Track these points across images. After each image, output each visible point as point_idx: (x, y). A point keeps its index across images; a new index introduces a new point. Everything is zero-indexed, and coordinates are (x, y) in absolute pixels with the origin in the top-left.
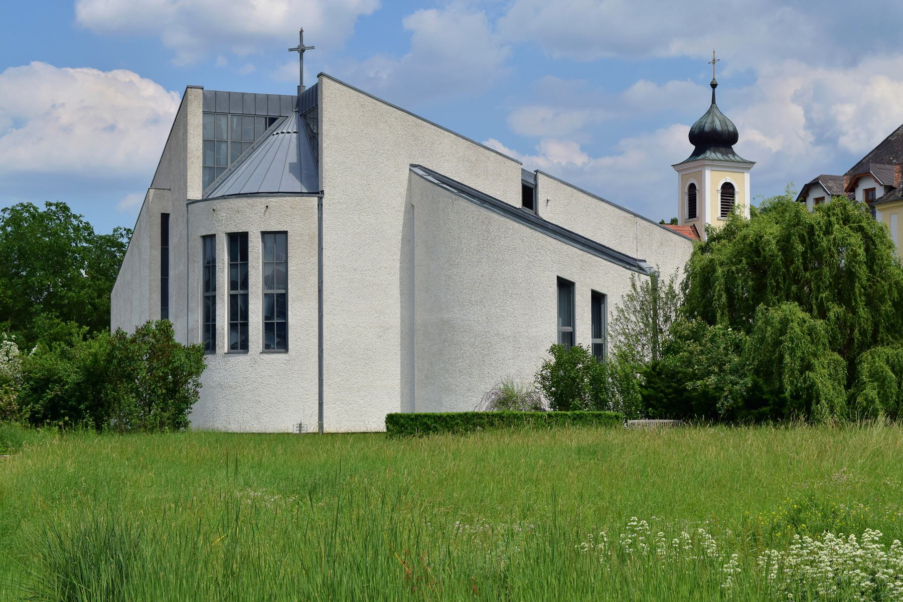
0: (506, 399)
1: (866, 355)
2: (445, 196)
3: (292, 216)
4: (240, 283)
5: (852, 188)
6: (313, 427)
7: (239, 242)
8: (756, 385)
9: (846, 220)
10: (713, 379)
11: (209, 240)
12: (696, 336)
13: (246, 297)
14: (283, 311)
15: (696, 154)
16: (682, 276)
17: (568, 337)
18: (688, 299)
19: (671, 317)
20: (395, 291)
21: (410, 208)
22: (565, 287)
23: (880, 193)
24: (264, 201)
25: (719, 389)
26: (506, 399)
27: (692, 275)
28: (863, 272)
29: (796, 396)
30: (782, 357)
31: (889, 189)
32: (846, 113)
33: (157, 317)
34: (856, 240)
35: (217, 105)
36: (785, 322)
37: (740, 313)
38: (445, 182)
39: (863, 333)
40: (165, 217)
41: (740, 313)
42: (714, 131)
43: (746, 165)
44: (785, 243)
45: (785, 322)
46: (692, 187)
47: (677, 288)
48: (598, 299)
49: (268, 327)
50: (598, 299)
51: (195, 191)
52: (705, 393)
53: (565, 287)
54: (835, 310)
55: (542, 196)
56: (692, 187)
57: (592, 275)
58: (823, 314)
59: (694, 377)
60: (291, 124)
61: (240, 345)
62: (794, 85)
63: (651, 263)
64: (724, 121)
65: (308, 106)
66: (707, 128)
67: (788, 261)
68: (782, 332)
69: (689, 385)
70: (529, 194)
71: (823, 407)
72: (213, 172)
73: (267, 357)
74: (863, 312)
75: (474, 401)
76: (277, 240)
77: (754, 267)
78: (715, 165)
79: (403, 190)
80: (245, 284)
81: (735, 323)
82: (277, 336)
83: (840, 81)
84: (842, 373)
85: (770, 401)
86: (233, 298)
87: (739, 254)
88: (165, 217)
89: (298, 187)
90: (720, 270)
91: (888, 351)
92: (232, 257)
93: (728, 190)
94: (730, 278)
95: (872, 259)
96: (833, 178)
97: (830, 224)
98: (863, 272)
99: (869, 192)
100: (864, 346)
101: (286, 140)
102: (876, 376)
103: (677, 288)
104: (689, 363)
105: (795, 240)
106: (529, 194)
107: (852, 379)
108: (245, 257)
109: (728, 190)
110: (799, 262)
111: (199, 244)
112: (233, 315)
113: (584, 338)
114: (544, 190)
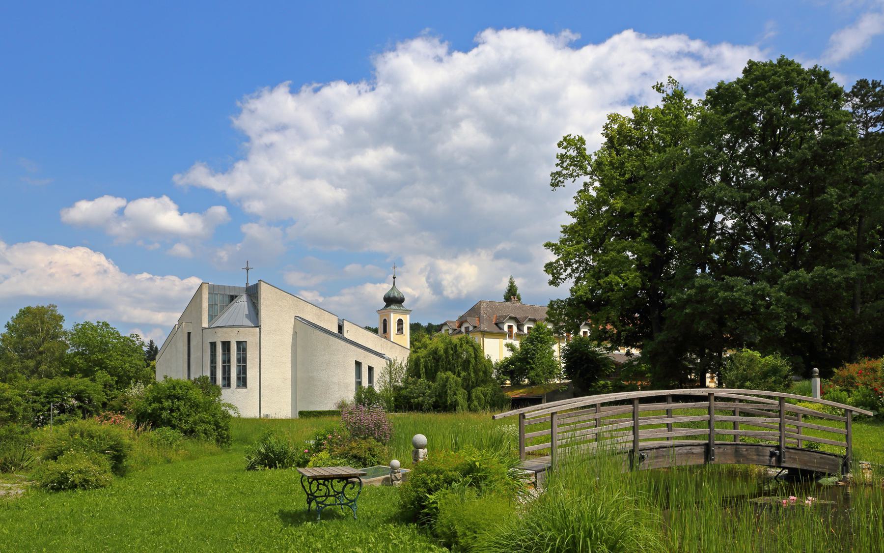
0: (343, 405)
1: (474, 390)
2: (311, 329)
3: (249, 336)
4: (227, 361)
5: (460, 326)
6: (257, 416)
7: (226, 345)
8: (437, 401)
9: (467, 343)
10: (421, 399)
11: (213, 345)
12: (414, 383)
13: (229, 367)
14: (245, 372)
15: (387, 306)
16: (405, 361)
17: (359, 384)
18: (408, 370)
19: (403, 374)
20: (289, 365)
21: (295, 333)
22: (358, 364)
23: (471, 329)
24: (237, 329)
25: (423, 402)
26: (343, 405)
27: (410, 360)
28: (473, 361)
29: (451, 405)
30: (446, 391)
31: (475, 327)
32: (447, 280)
33: (208, 374)
34: (471, 350)
35: (213, 290)
36: (447, 378)
37: (431, 375)
38: (310, 324)
39: (473, 382)
40: (189, 334)
41: (431, 375)
42: (395, 297)
43: (408, 312)
44: (446, 351)
45: (447, 378)
46: (385, 320)
47: (403, 365)
48: (370, 369)
49: (239, 378)
50: (370, 369)
51: (205, 325)
52: (418, 403)
53: (358, 364)
54: (463, 374)
55: (346, 329)
56: (385, 320)
57: (368, 360)
58: (459, 376)
59: (414, 398)
60: (244, 298)
61: (228, 385)
62: (422, 265)
63: (387, 355)
64: (399, 292)
65: (253, 293)
66: (392, 296)
67: (447, 357)
68: (447, 382)
69: (412, 401)
70: (340, 328)
71: (459, 408)
72: (212, 317)
73: (238, 390)
74: (472, 375)
75: (331, 406)
76: (242, 347)
77: (434, 358)
78: (395, 312)
79: (292, 326)
80: (229, 361)
81: (428, 379)
82: (243, 381)
83: (442, 264)
84: (466, 396)
85: (442, 405)
86: (224, 367)
87: (430, 354)
88: (189, 334)
89: (250, 324)
90: (422, 360)
91: (481, 388)
92: (224, 351)
93: (400, 322)
94: (426, 362)
95: (476, 357)
96: (452, 322)
97: (461, 344)
98: (473, 361)
99: (467, 328)
100: (473, 387)
101: (242, 303)
102: (478, 398)
103: (403, 365)
104: (411, 392)
105: (450, 350)
106: (340, 328)
107: (469, 399)
108: (229, 350)
109: (400, 322)
110: (450, 357)
111: (209, 346)
112: (224, 373)
113: (365, 383)
114: (347, 326)
